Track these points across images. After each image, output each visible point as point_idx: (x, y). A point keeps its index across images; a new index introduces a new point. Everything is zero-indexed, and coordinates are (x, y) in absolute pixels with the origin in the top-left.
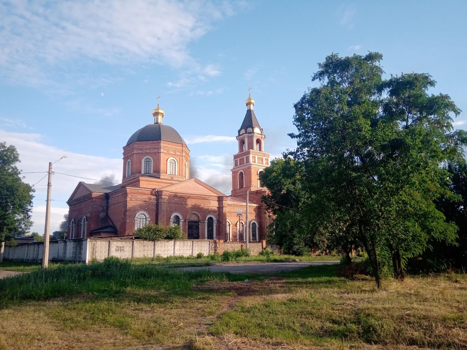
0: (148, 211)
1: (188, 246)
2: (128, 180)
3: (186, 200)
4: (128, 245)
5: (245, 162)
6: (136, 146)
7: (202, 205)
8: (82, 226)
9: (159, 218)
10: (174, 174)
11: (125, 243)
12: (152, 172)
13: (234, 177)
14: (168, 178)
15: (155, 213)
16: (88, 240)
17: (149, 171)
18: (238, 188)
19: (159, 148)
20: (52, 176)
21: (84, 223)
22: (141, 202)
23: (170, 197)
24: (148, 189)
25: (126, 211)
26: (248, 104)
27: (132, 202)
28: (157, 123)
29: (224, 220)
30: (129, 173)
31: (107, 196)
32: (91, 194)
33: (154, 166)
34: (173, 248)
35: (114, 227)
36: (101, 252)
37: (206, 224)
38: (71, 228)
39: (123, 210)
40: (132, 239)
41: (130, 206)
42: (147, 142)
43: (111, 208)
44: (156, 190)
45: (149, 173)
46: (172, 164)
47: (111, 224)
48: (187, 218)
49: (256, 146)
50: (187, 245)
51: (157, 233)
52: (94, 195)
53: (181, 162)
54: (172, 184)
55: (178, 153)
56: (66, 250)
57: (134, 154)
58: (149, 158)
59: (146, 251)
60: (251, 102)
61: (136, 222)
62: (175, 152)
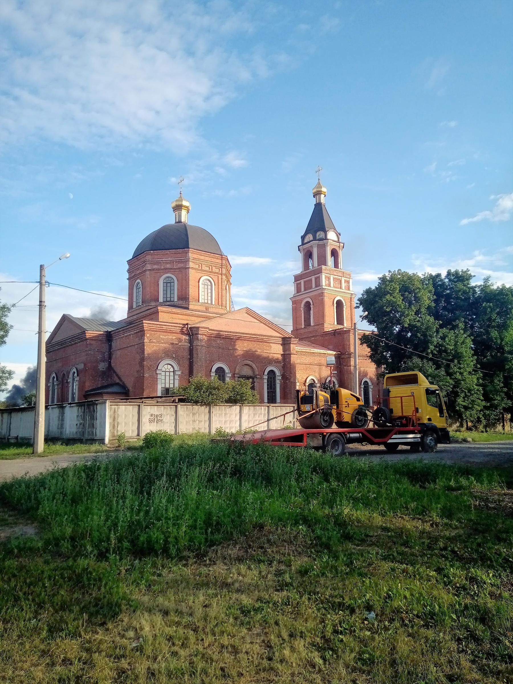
0: (176, 359)
1: (261, 414)
2: (138, 312)
3: (235, 342)
4: (169, 411)
5: (314, 286)
6: (149, 258)
7: (259, 352)
8: (71, 384)
9: (195, 371)
10: (209, 302)
11: (164, 408)
12: (176, 300)
13: (295, 311)
14: (203, 309)
15: (188, 363)
16: (108, 403)
17: (170, 297)
18: (303, 327)
19: (187, 261)
20: (47, 290)
21: (53, 383)
22: (167, 345)
23: (210, 337)
24: (176, 325)
25: (143, 359)
26: (317, 194)
27: (152, 344)
28: (180, 222)
29: (292, 375)
30: (138, 299)
31: (109, 337)
32: (84, 333)
33: (178, 290)
34: (238, 417)
35: (123, 386)
36: (126, 423)
37: (266, 381)
38: (51, 388)
39: (138, 357)
40: (174, 401)
41: (150, 352)
42: (168, 252)
43: (117, 355)
44: (189, 326)
45: (170, 301)
46: (206, 287)
47: (118, 381)
48: (237, 370)
49: (330, 261)
50: (259, 412)
51: (214, 392)
52: (89, 334)
53: (220, 284)
54: (209, 318)
55: (215, 270)
56: (63, 420)
57: (145, 271)
58: (171, 277)
59: (197, 422)
60: (321, 191)
61: (159, 377)
62: (211, 267)
